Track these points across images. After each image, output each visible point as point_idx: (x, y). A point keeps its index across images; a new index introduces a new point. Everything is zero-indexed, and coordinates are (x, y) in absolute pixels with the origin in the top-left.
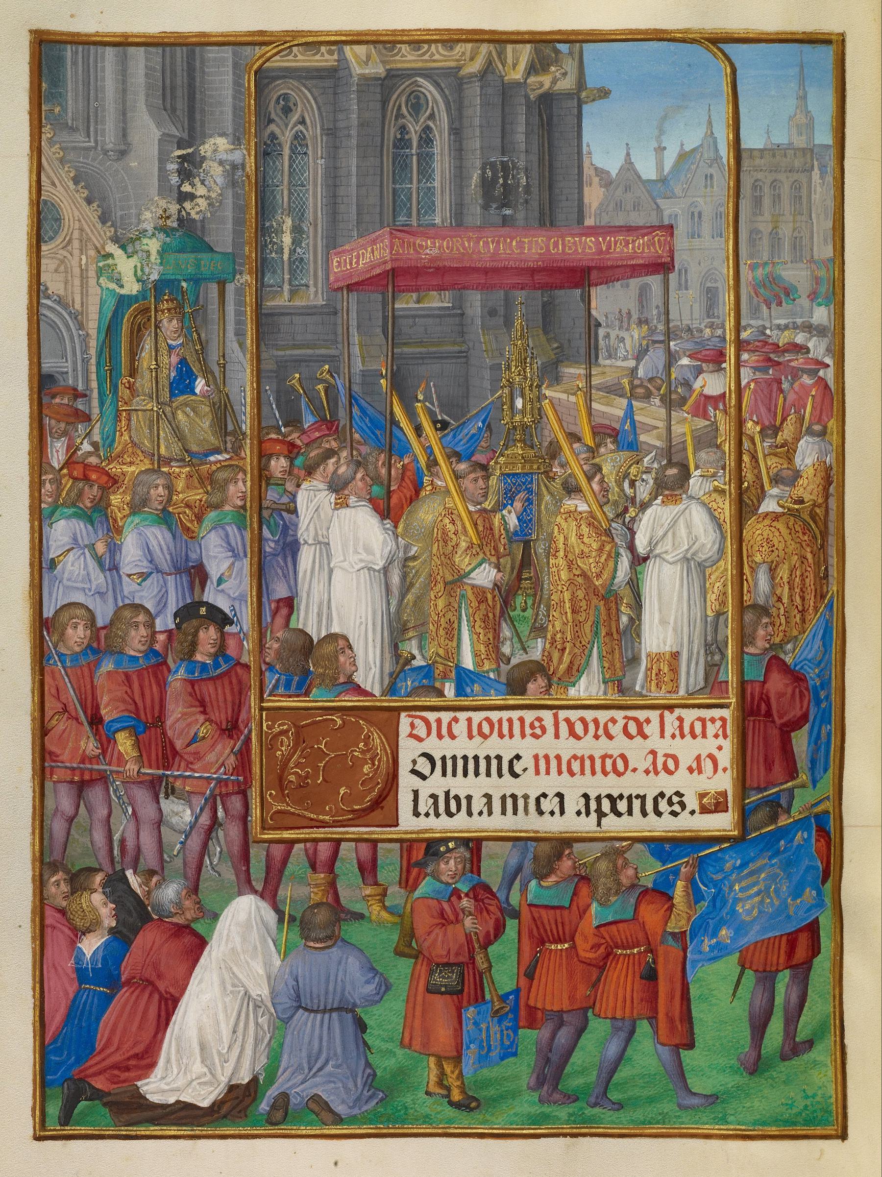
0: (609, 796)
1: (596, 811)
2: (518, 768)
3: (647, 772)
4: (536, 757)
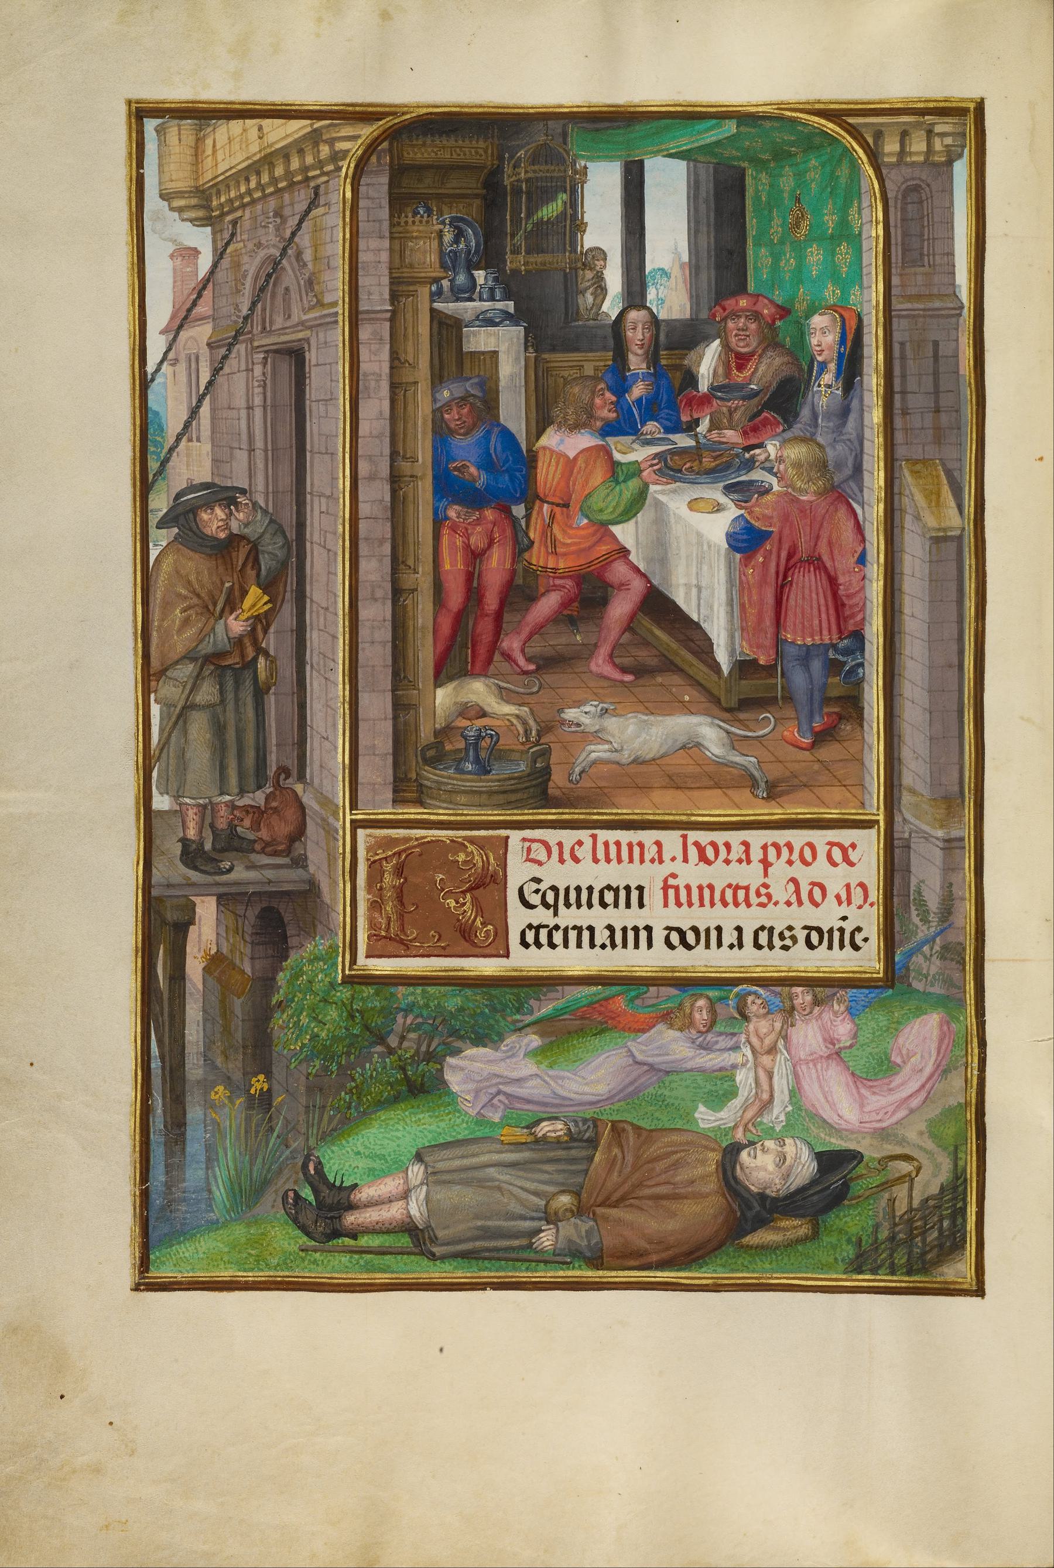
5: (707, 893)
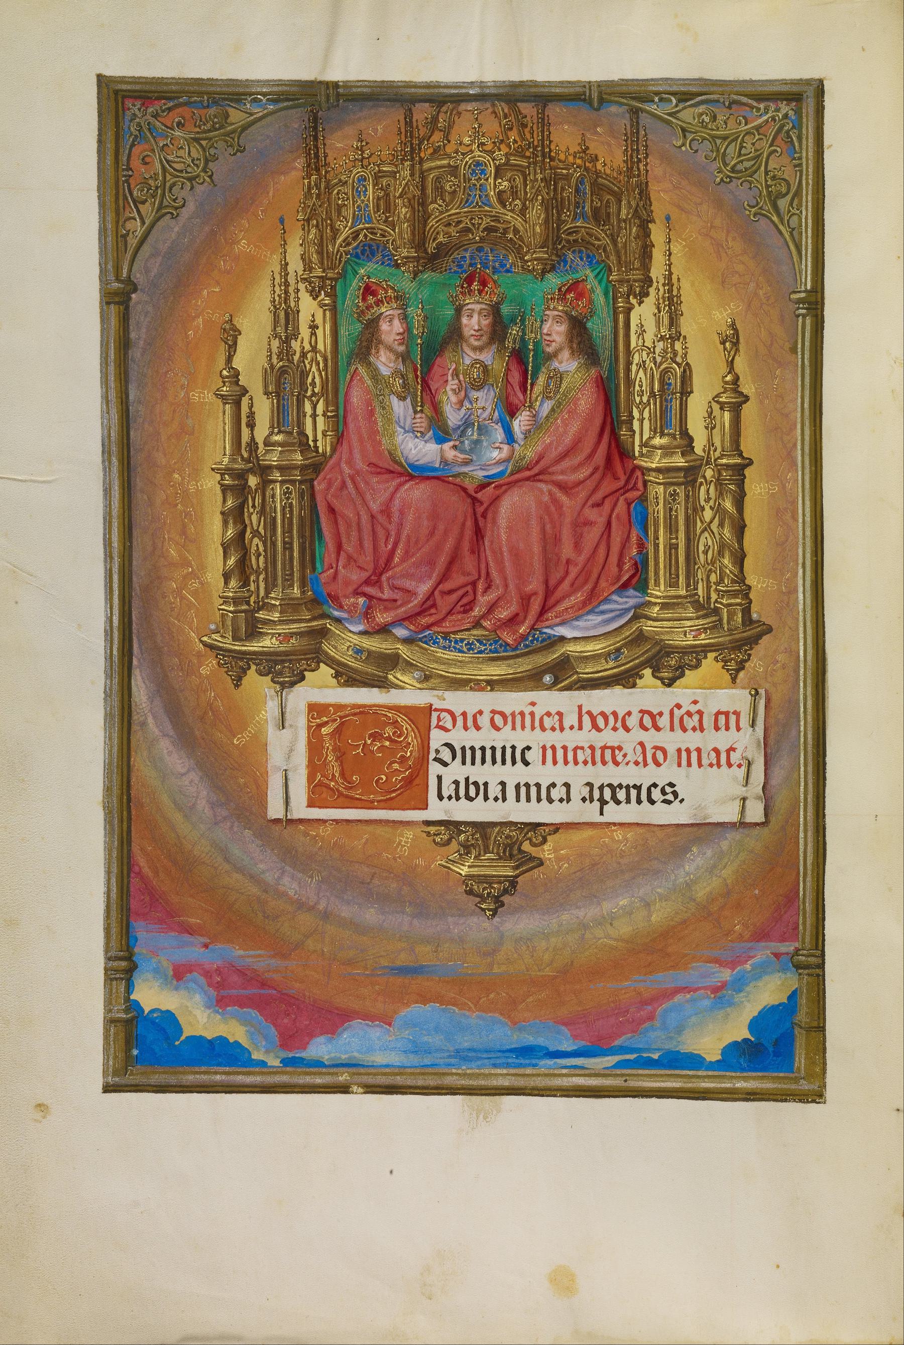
0: (610, 785)
4: (544, 748)
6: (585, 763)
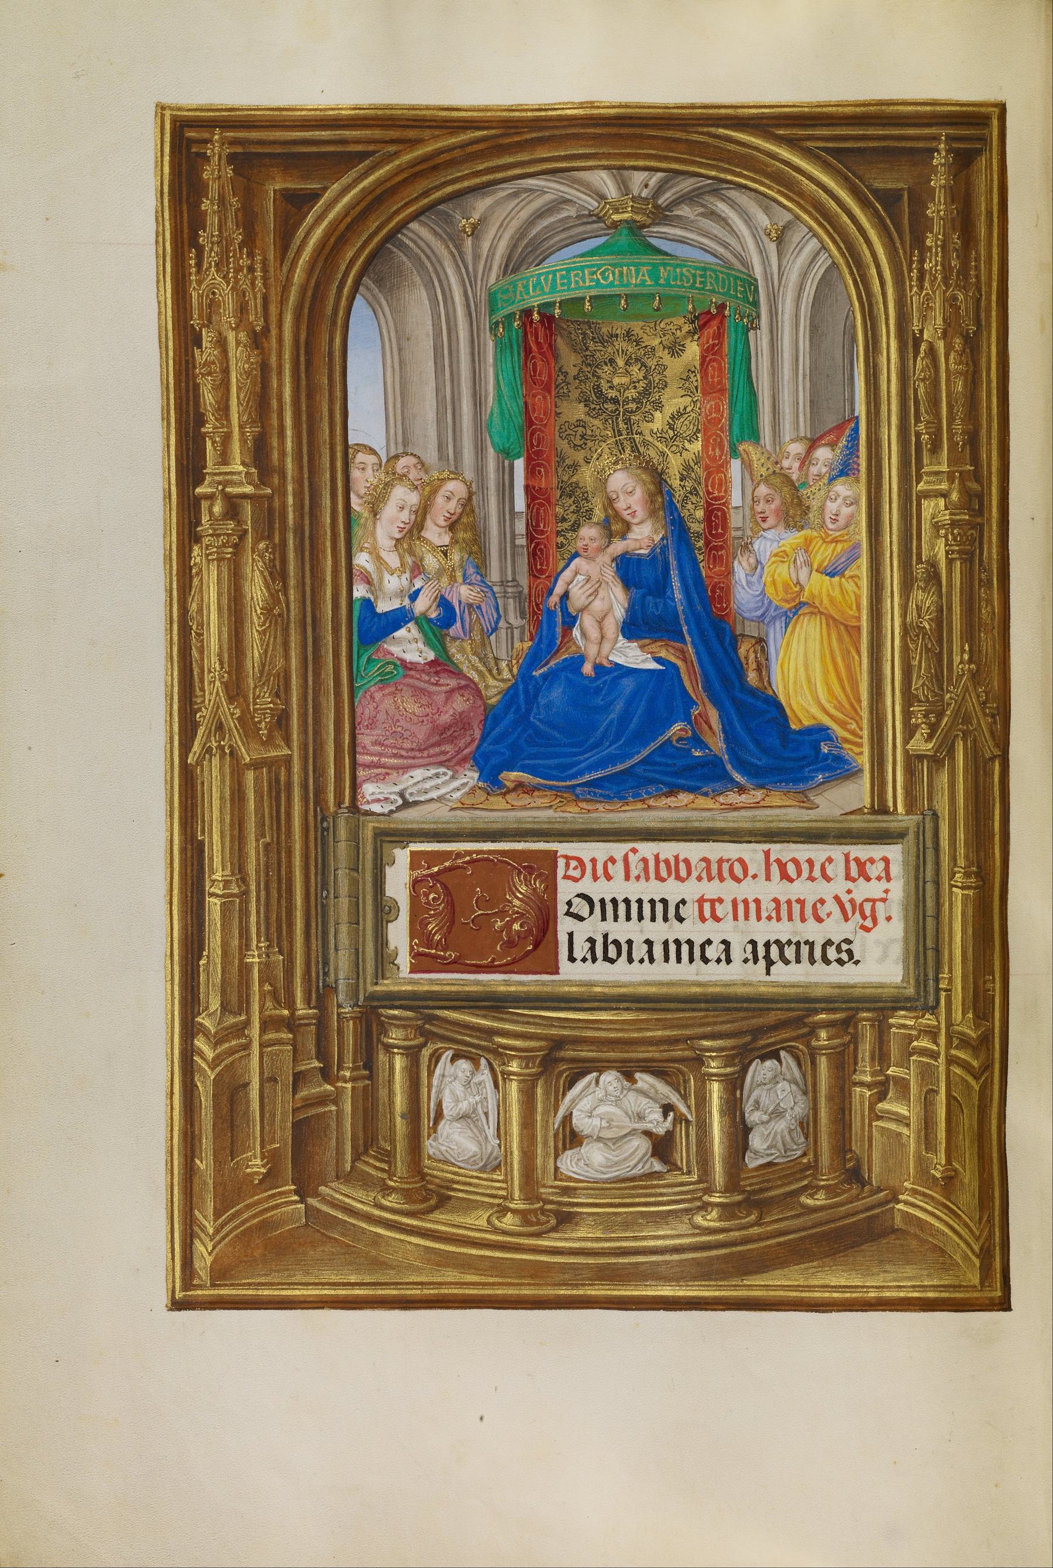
1: (764, 957)
2: (822, 914)
3: (719, 961)
5: (659, 907)
6: (769, 918)
